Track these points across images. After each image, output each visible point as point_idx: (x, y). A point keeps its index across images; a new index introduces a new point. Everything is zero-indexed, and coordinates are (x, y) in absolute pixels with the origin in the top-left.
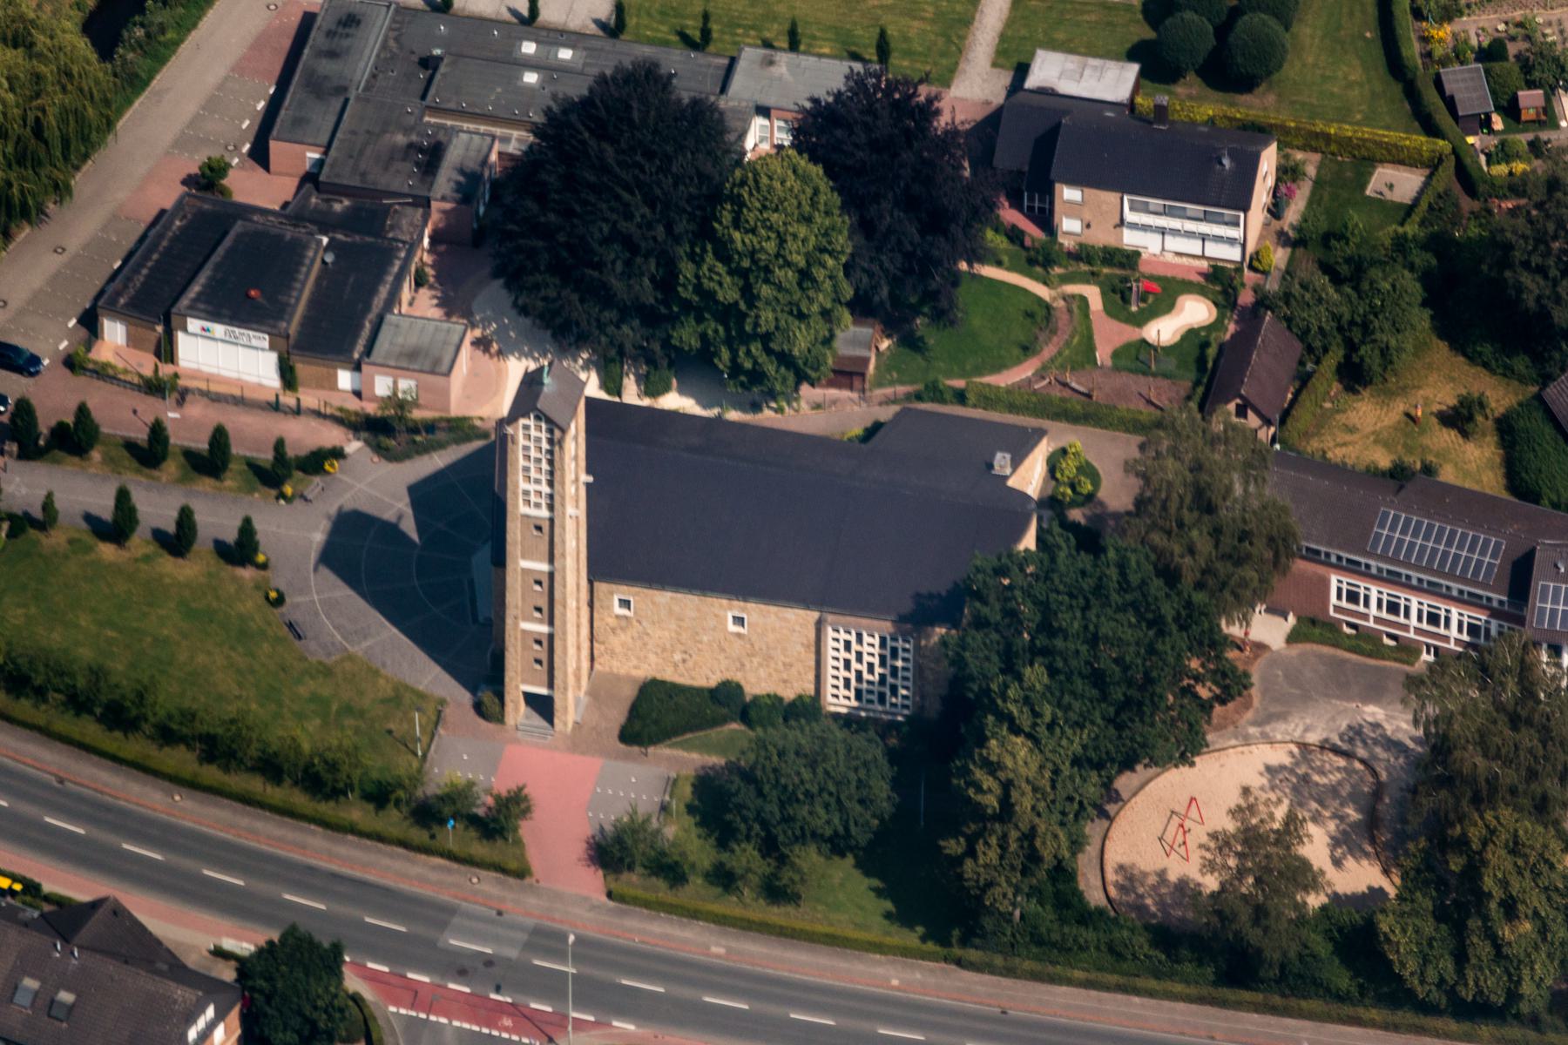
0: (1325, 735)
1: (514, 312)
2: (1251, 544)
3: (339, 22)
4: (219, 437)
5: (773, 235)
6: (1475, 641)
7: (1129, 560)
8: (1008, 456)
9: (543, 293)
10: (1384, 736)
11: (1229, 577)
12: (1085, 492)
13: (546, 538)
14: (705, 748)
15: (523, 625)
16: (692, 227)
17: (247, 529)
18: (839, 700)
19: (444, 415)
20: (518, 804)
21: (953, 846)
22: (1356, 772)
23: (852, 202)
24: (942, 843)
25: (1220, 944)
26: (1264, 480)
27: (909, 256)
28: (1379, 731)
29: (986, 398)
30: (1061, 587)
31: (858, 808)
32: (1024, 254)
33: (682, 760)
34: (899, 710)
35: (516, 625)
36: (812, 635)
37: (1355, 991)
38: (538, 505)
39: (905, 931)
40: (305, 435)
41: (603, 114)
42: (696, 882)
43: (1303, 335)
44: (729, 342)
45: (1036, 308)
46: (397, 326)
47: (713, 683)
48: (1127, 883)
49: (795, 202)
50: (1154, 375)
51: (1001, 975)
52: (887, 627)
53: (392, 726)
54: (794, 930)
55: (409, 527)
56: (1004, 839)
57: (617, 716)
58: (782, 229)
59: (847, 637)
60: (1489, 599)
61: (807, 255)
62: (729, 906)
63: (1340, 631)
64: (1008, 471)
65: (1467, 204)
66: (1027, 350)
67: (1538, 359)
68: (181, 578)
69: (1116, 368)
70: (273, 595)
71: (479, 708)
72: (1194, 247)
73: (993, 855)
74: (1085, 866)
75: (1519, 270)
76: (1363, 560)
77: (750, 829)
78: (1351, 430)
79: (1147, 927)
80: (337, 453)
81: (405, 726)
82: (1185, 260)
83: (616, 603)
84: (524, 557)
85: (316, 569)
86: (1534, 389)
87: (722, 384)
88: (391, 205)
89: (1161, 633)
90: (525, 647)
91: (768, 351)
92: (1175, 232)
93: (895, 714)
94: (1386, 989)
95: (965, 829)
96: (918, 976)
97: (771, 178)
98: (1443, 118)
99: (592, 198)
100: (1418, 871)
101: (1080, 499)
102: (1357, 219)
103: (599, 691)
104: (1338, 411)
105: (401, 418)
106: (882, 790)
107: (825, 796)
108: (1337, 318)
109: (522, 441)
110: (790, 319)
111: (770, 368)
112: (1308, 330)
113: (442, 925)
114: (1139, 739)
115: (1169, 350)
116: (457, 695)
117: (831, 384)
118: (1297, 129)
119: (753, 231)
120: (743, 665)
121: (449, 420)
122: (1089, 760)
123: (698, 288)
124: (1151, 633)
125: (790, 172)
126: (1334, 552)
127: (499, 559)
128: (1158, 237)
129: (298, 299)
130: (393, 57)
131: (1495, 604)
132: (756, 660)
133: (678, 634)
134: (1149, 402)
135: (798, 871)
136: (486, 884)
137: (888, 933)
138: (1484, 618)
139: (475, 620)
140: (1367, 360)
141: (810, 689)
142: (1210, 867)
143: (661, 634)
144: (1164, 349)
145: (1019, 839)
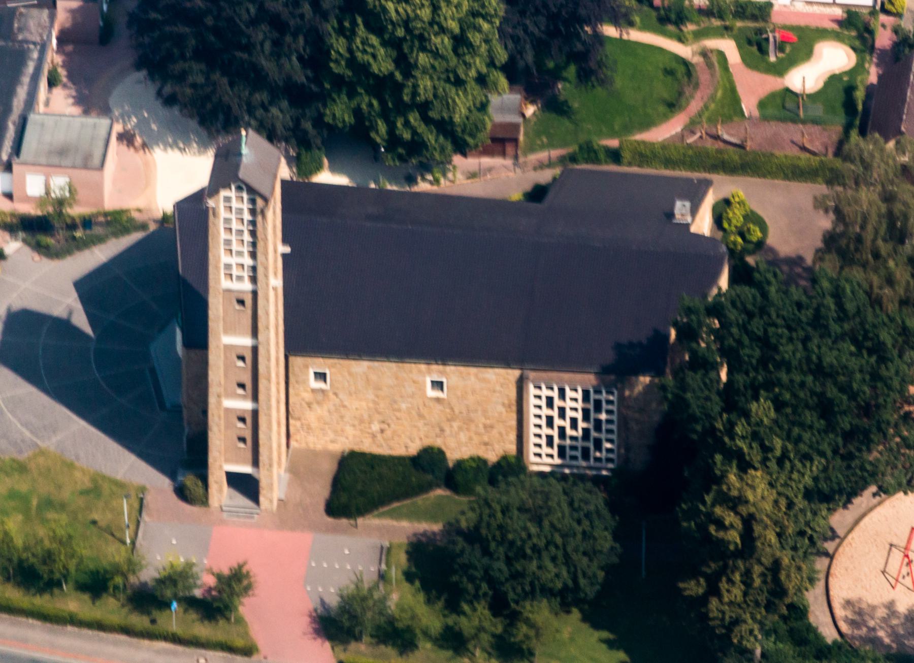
1: (158, 104)
7: (844, 290)
8: (688, 204)
9: (190, 79)
12: (754, 239)
13: (249, 312)
14: (414, 515)
15: (226, 403)
19: (101, 210)
21: (694, 588)
24: (681, 585)
29: (641, 155)
30: (780, 322)
31: (585, 560)
33: (390, 530)
34: (604, 464)
35: (219, 403)
36: (513, 393)
38: (240, 278)
45: (674, 65)
46: (43, 125)
47: (413, 449)
48: (856, 618)
50: (804, 122)
52: (590, 379)
53: (96, 516)
55: (81, 321)
56: (747, 574)
57: (321, 491)
59: (549, 393)
61: (460, 21)
66: (673, 106)
69: (765, 118)
71: (182, 493)
73: (737, 592)
77: (478, 588)
81: (109, 516)
83: (312, 376)
84: (226, 332)
87: (376, 157)
88: (15, 9)
90: (228, 426)
91: (426, 120)
93: (599, 469)
95: (704, 569)
101: (750, 247)
103: (298, 469)
105: (60, 214)
106: (605, 541)
107: (552, 549)
109: (223, 213)
110: (448, 86)
111: (430, 137)
114: (868, 467)
115: (814, 97)
116: (157, 483)
120: (442, 430)
121: (106, 214)
122: (820, 492)
123: (352, 62)
124: (873, 360)
127: (198, 339)
132: (455, 425)
133: (375, 402)
134: (803, 149)
135: (531, 625)
141: (512, 448)
143: (358, 405)
144: (809, 96)
145: (763, 575)
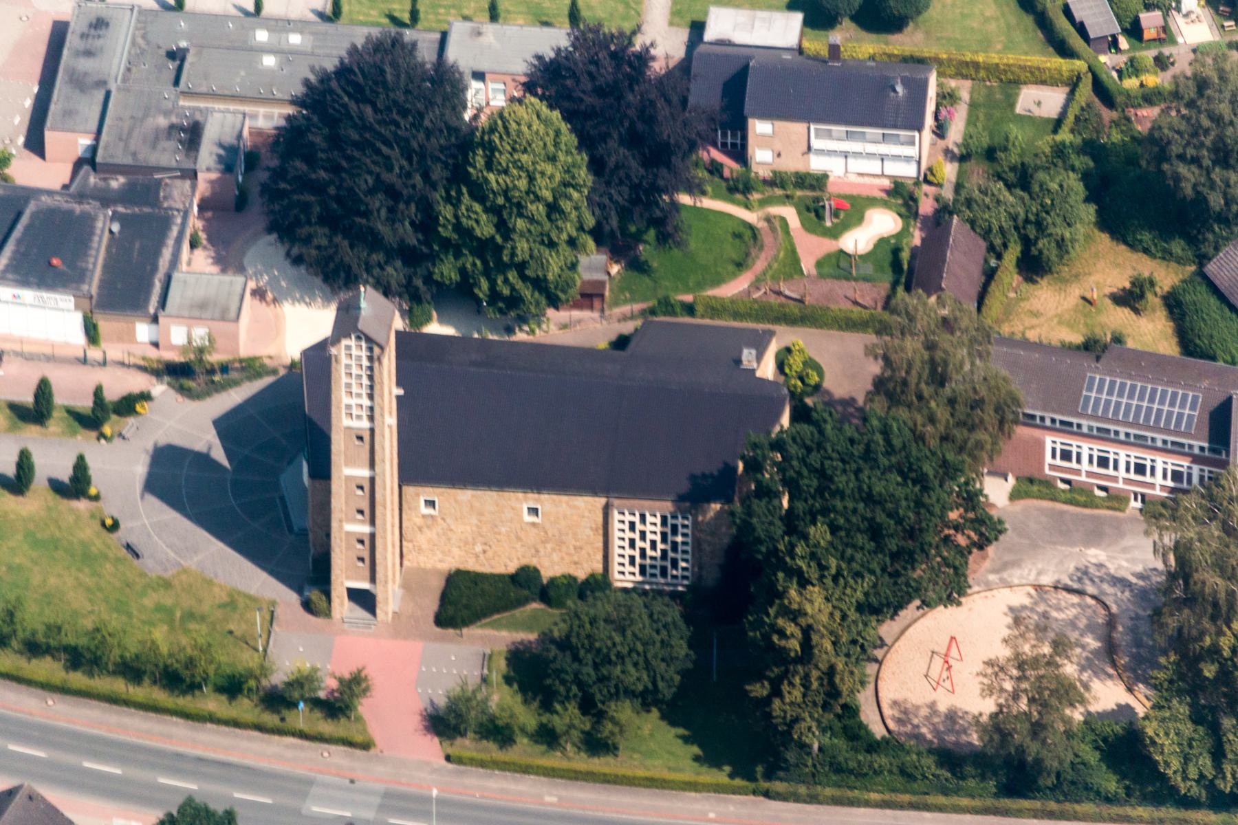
0: (1056, 577)
2: (982, 410)
3: (91, 26)
4: (43, 391)
5: (523, 175)
6: (1179, 485)
7: (891, 427)
8: (754, 352)
10: (1109, 574)
11: (965, 441)
12: (812, 383)
14: (513, 626)
15: (347, 527)
16: (446, 174)
17: (81, 467)
18: (625, 577)
20: (359, 683)
21: (759, 690)
22: (1089, 607)
23: (586, 142)
24: (748, 688)
25: (1002, 763)
26: (988, 353)
27: (635, 188)
28: (1103, 570)
29: (713, 308)
30: (835, 455)
31: (663, 665)
32: (724, 184)
33: (493, 639)
34: (680, 581)
35: (341, 527)
36: (600, 519)
37: (1122, 792)
38: (359, 417)
39: (714, 770)
40: (118, 384)
41: (360, 79)
42: (523, 741)
43: (986, 234)
44: (487, 273)
45: (742, 229)
46: (185, 282)
47: (512, 568)
48: (902, 716)
49: (541, 143)
50: (856, 280)
51: (805, 802)
52: (667, 506)
53: (232, 627)
54: (616, 776)
55: (219, 455)
56: (806, 678)
58: (531, 168)
59: (632, 518)
60: (1191, 447)
61: (553, 190)
62: (554, 760)
63: (1055, 487)
64: (755, 365)
65: (1107, 115)
67: (1193, 242)
68: (24, 513)
69: (821, 276)
70: (109, 522)
71: (307, 606)
72: (874, 167)
73: (797, 694)
74: (864, 699)
75: (1175, 162)
76: (1075, 420)
77: (568, 690)
78: (1036, 314)
79: (930, 751)
80: (145, 397)
81: (244, 626)
82: (867, 180)
83: (422, 503)
84: (347, 465)
85: (142, 497)
86: (1193, 268)
87: (479, 311)
88: (161, 179)
89: (926, 489)
91: (523, 277)
92: (857, 155)
93: (676, 585)
94: (1150, 788)
96: (732, 808)
97: (519, 124)
98: (1076, 41)
99: (356, 154)
100: (1171, 682)
101: (809, 389)
102: (1017, 133)
104: (1022, 300)
106: (681, 648)
107: (634, 655)
108: (1014, 218)
109: (344, 360)
110: (542, 248)
111: (527, 293)
112: (990, 230)
113: (304, 795)
114: (913, 584)
115: (864, 258)
116: (287, 598)
117: (577, 306)
118: (950, 60)
119: (506, 172)
120: (537, 551)
121: (241, 361)
122: (870, 606)
123: (458, 227)
124: (917, 489)
125: (535, 117)
126: (1048, 416)
127: (322, 470)
128: (842, 160)
129: (95, 264)
130: (143, 52)
131: (1196, 451)
132: (549, 546)
134: (856, 303)
135: (615, 722)
136: (336, 756)
137: (698, 774)
138: (1186, 464)
139: (291, 529)
140: (1045, 252)
141: (599, 567)
142: (989, 690)
143: (464, 529)
144: (861, 257)
145: (820, 678)
